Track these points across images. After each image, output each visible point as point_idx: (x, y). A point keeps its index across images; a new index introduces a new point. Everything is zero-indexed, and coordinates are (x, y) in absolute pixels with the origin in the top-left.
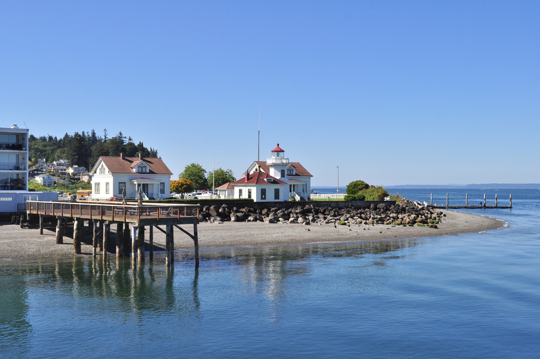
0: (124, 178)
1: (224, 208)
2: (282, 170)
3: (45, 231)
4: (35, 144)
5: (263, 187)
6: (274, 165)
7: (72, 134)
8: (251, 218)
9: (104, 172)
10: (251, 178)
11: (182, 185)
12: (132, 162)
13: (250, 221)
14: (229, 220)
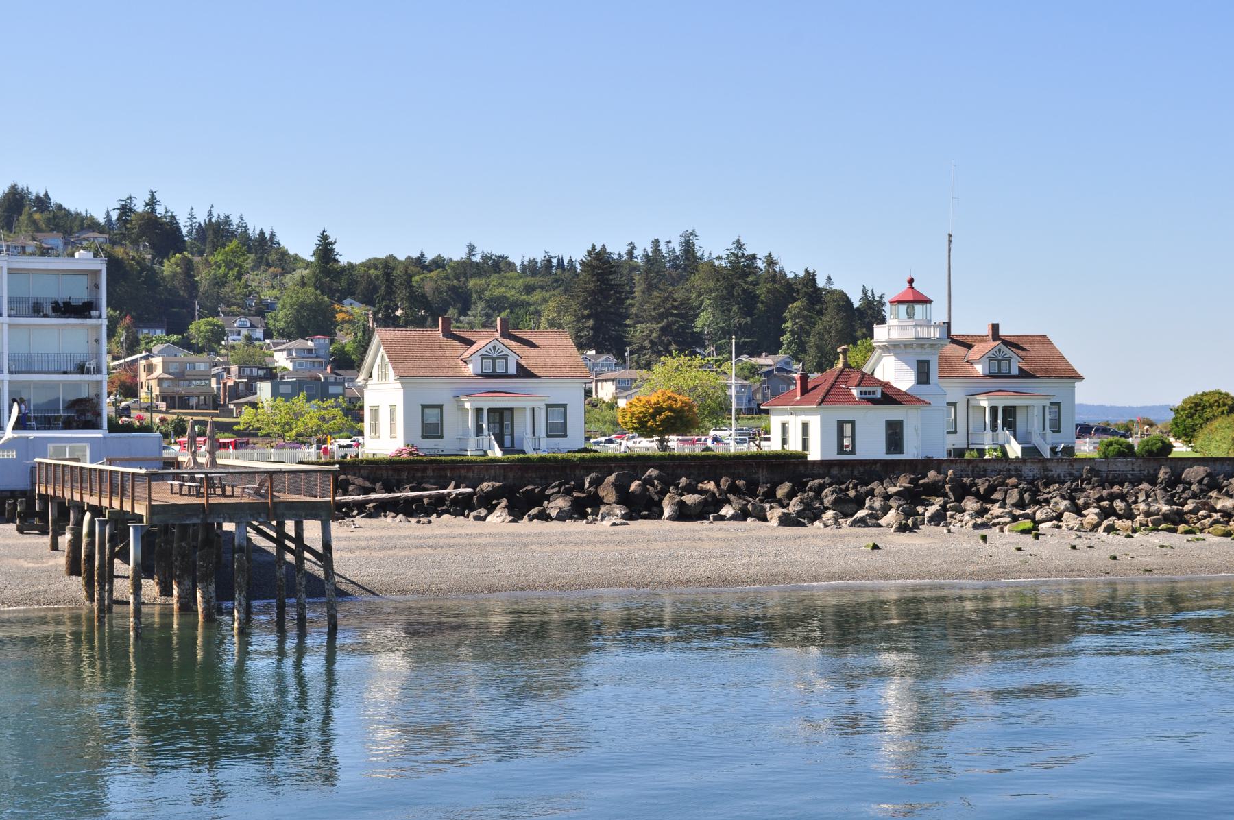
0: (438, 392)
1: (649, 481)
2: (919, 362)
4: (500, 285)
5: (845, 413)
7: (714, 247)
8: (727, 511)
11: (658, 410)
12: (470, 343)
13: (722, 518)
14: (659, 515)
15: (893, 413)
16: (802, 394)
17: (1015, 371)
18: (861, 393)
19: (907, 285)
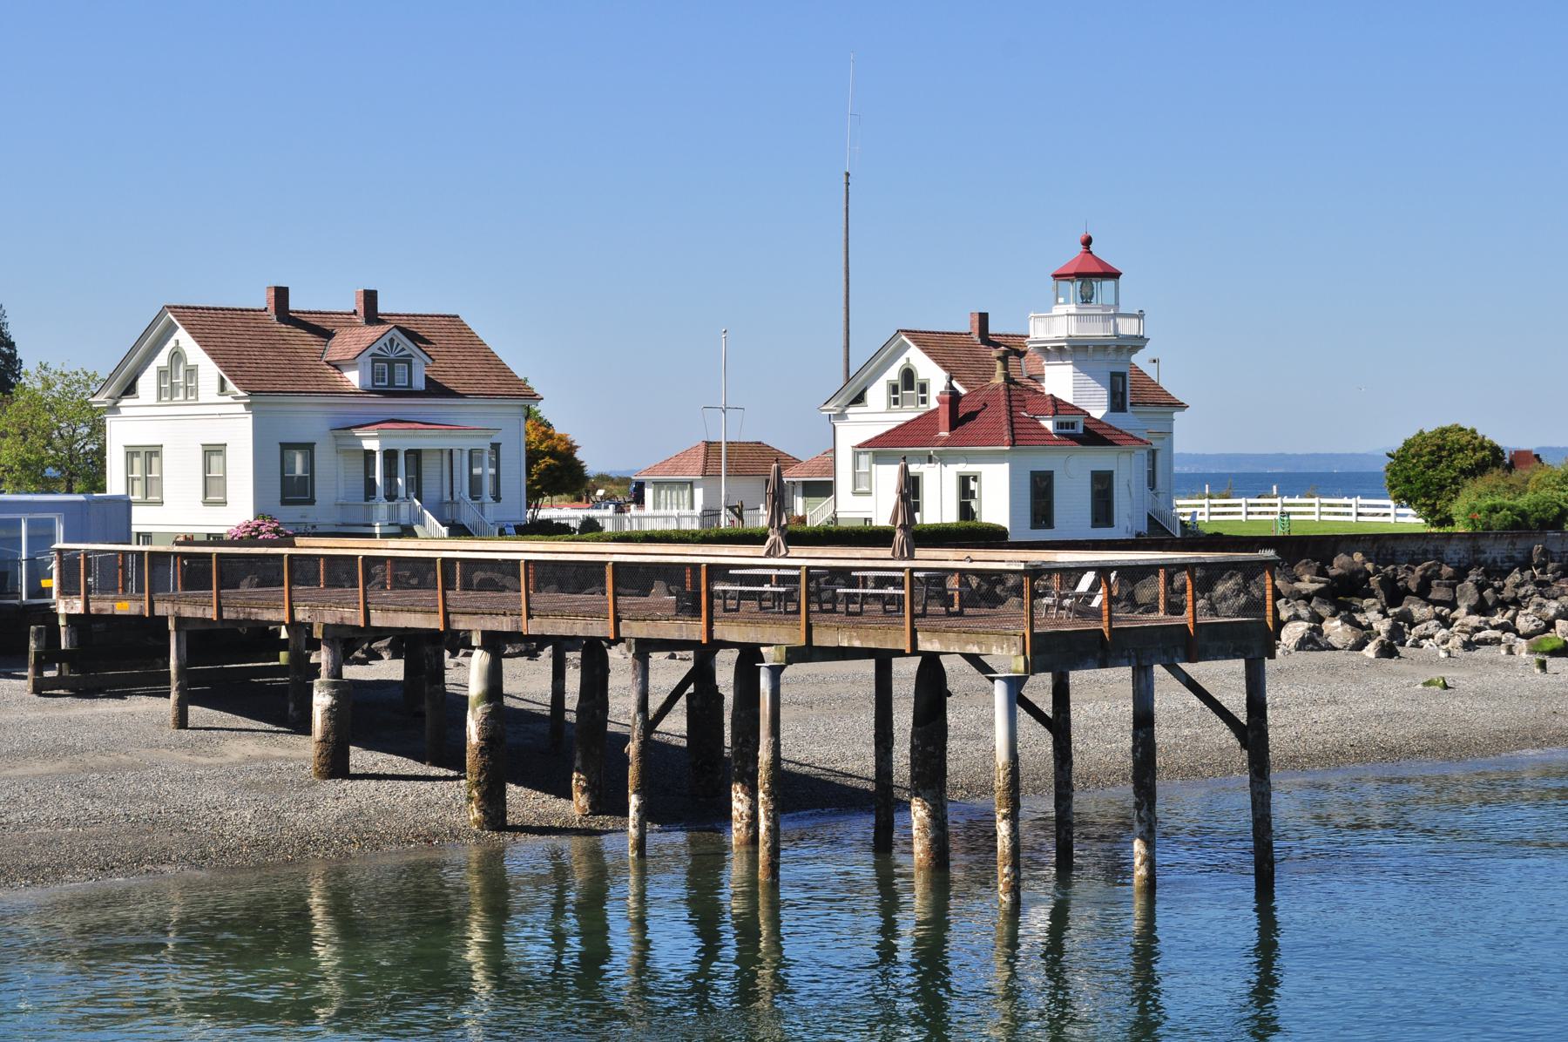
2: (1113, 375)
3: (196, 713)
5: (1042, 461)
6: (1074, 351)
9: (192, 391)
10: (971, 416)
15: (1100, 459)
16: (952, 428)
17: (419, 384)
18: (1060, 425)
19: (1081, 248)
